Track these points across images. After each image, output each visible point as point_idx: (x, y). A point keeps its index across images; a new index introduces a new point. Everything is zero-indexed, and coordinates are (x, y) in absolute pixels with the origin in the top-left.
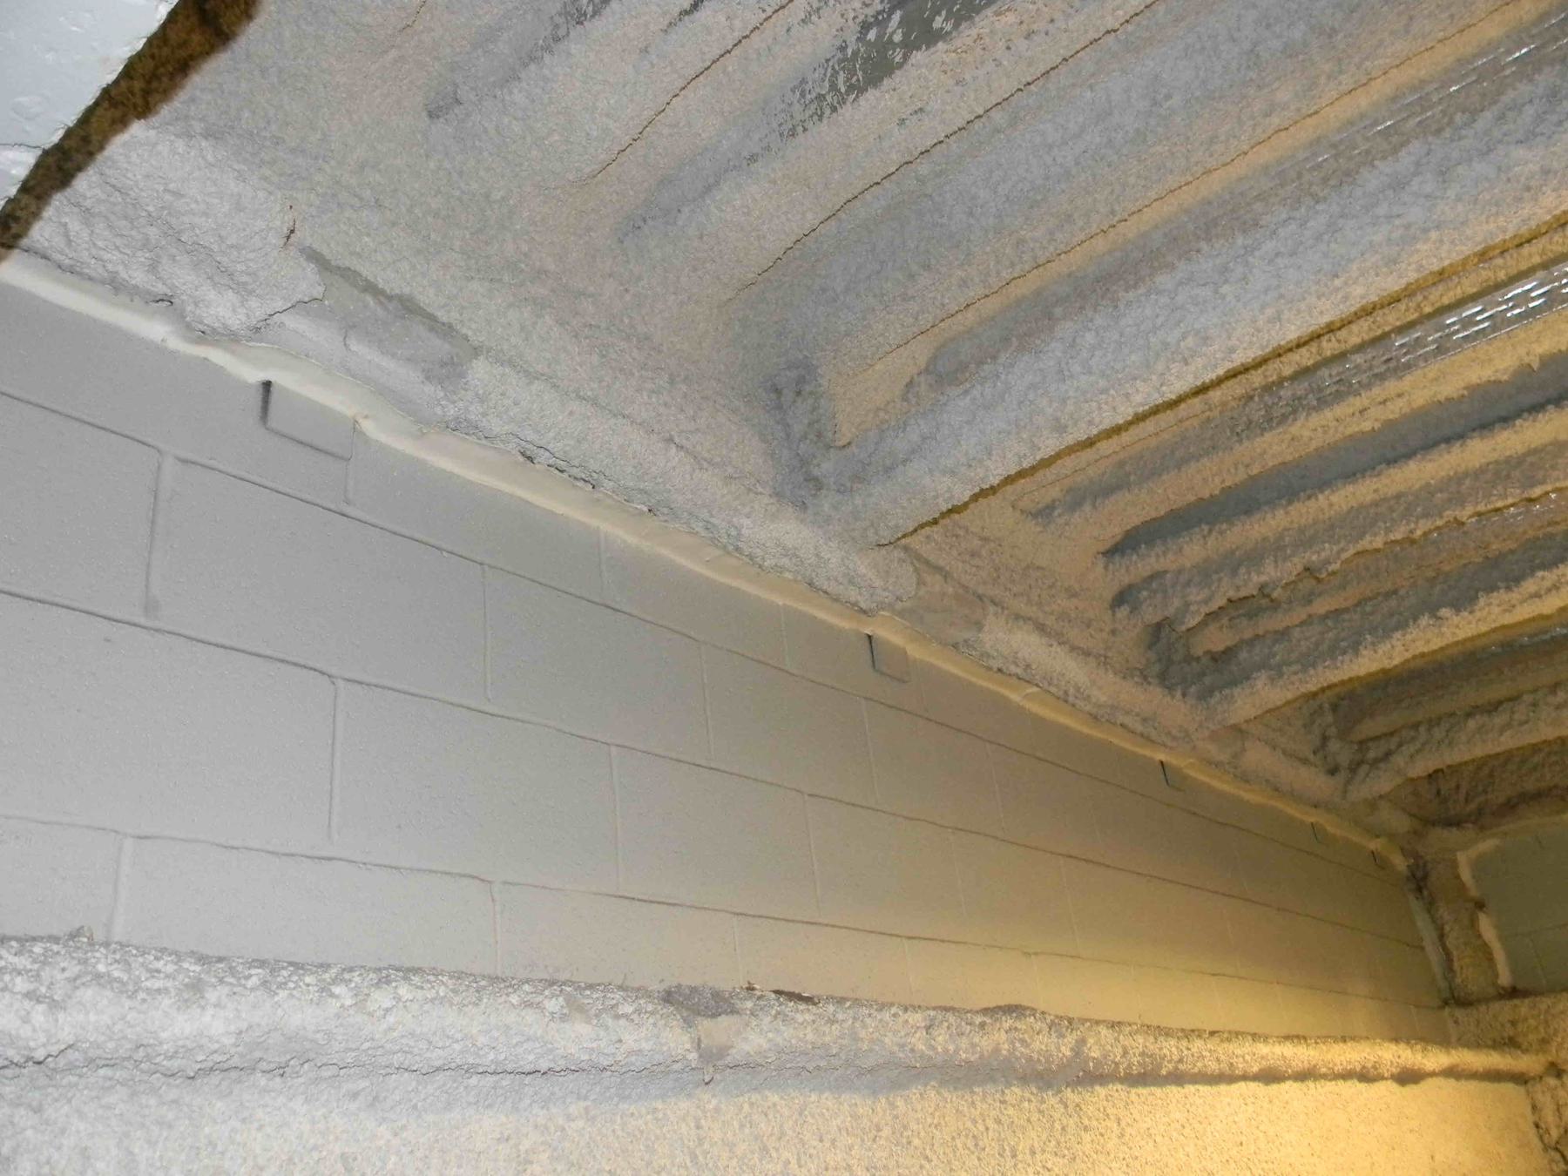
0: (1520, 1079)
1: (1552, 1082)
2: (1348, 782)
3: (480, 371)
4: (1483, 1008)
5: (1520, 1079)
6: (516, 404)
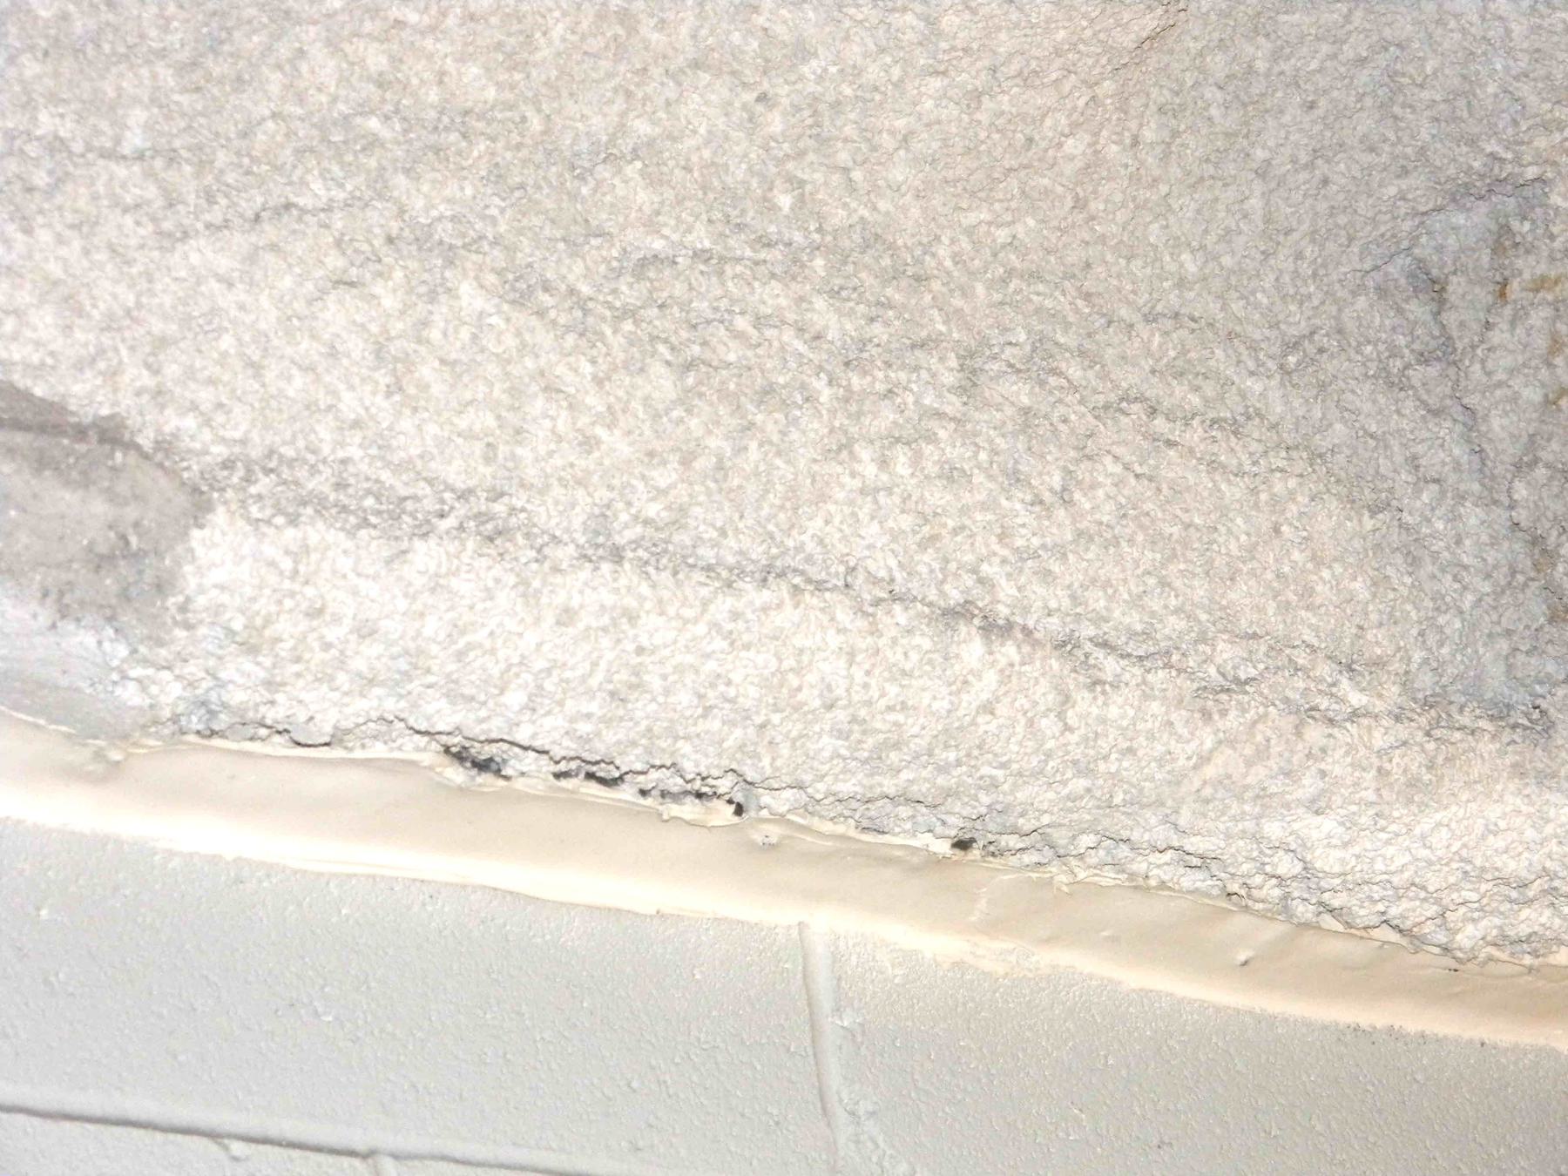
3: (223, 560)
6: (366, 631)
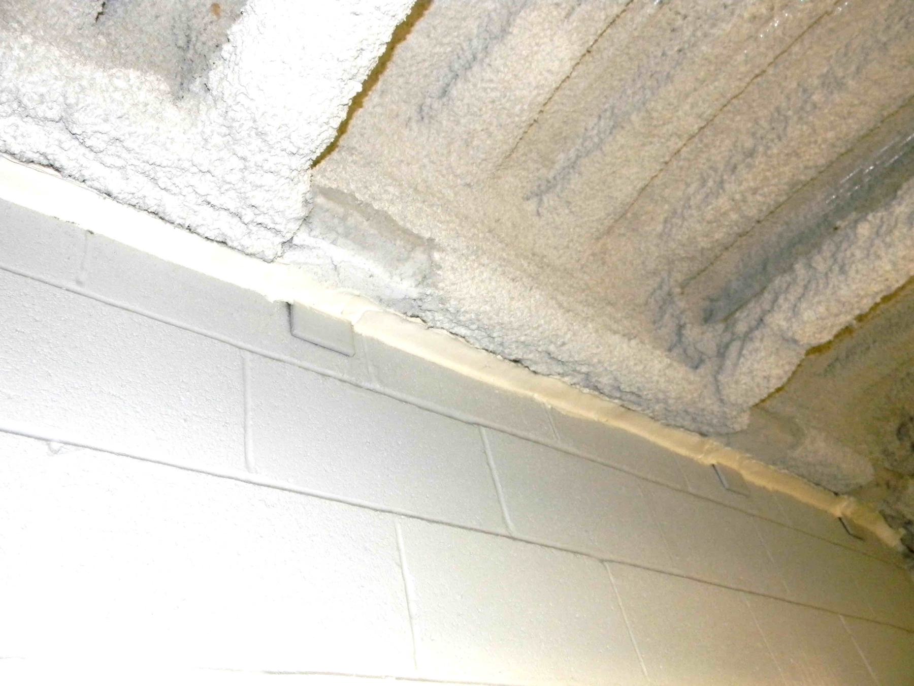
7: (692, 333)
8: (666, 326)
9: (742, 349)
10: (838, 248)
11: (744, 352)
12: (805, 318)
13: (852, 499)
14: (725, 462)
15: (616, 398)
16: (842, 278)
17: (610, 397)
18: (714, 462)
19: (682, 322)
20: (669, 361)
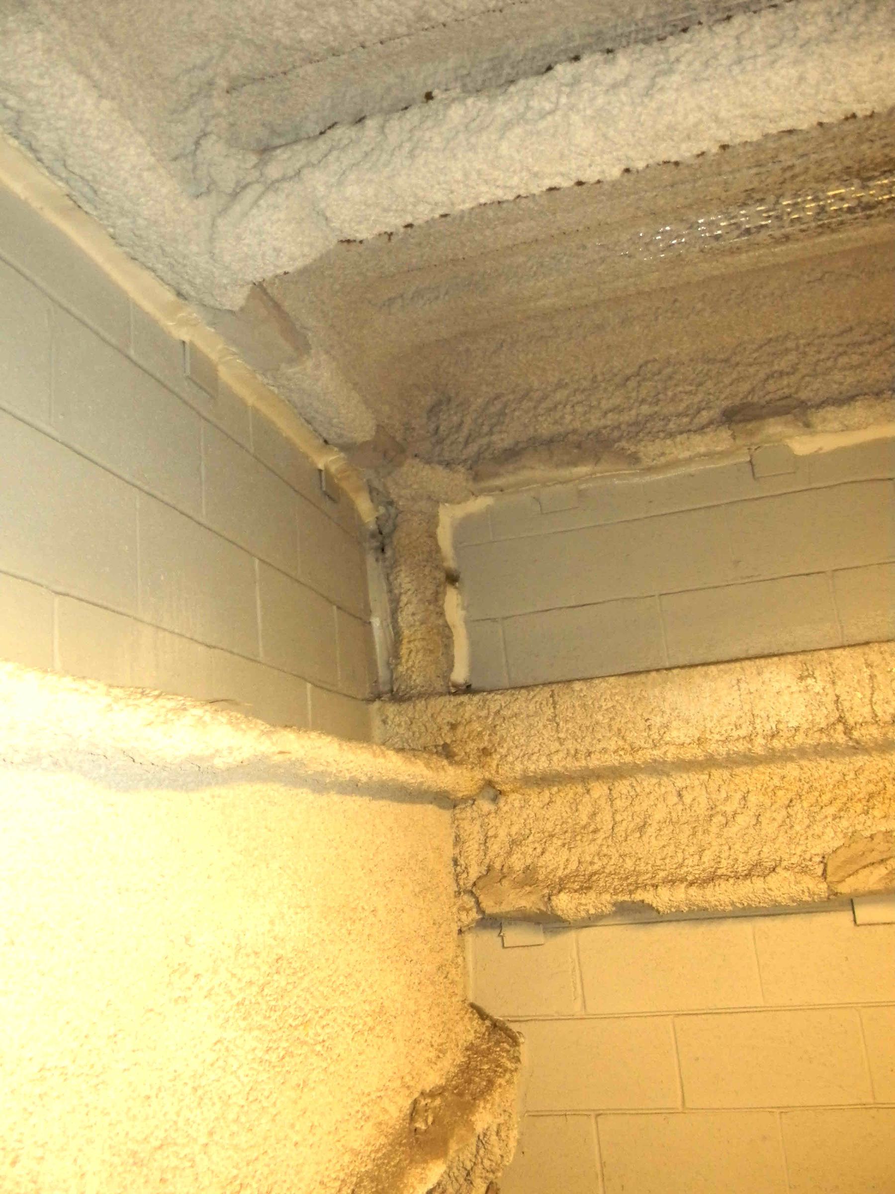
0: (445, 800)
1: (486, 806)
2: (224, 211)
4: (420, 704)
5: (445, 800)
7: (213, 148)
8: (185, 124)
9: (260, 198)
10: (422, 122)
11: (262, 202)
12: (348, 194)
13: (342, 455)
14: (201, 344)
15: (61, 179)
16: (407, 163)
17: (52, 171)
18: (186, 338)
19: (209, 129)
20: (153, 160)
